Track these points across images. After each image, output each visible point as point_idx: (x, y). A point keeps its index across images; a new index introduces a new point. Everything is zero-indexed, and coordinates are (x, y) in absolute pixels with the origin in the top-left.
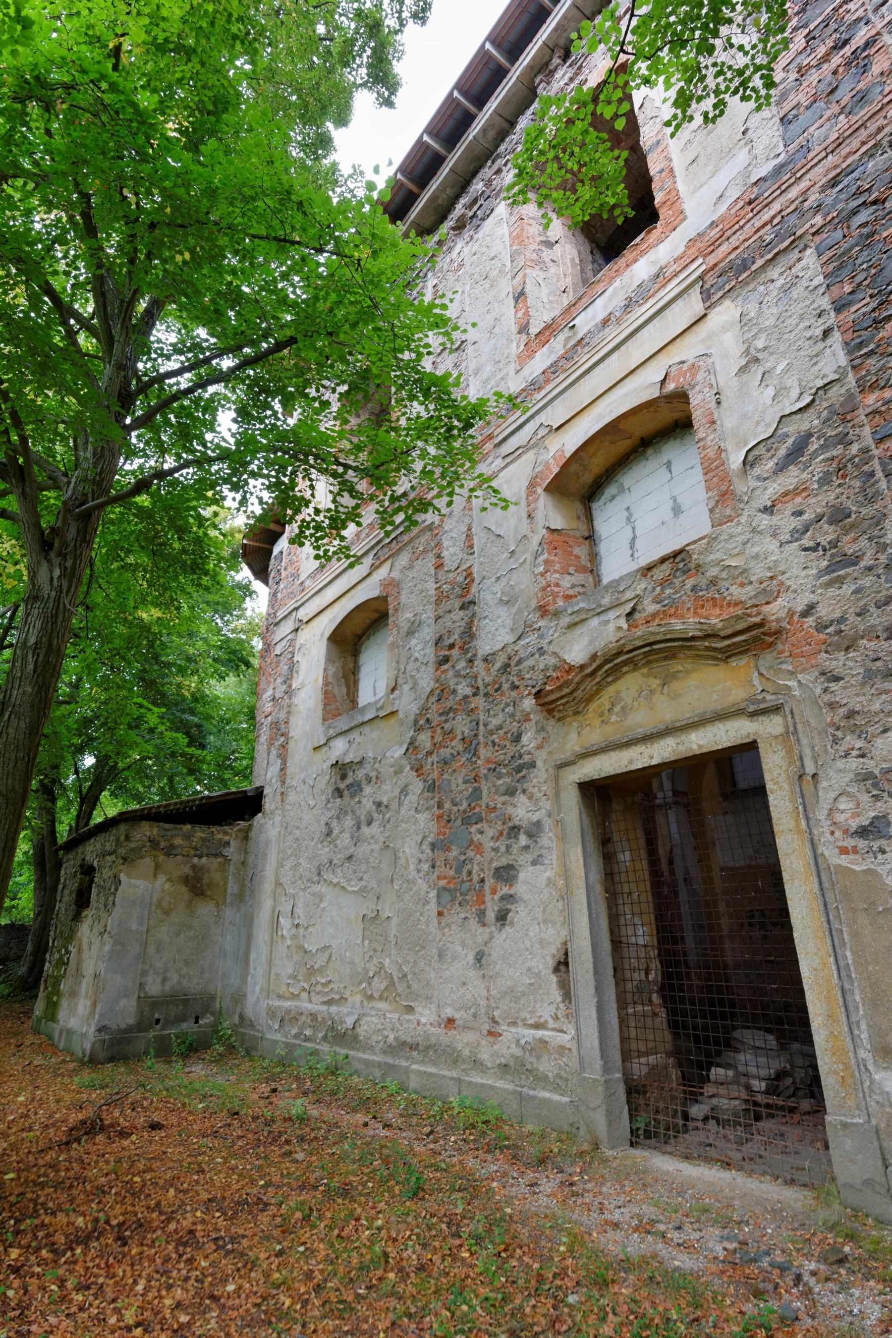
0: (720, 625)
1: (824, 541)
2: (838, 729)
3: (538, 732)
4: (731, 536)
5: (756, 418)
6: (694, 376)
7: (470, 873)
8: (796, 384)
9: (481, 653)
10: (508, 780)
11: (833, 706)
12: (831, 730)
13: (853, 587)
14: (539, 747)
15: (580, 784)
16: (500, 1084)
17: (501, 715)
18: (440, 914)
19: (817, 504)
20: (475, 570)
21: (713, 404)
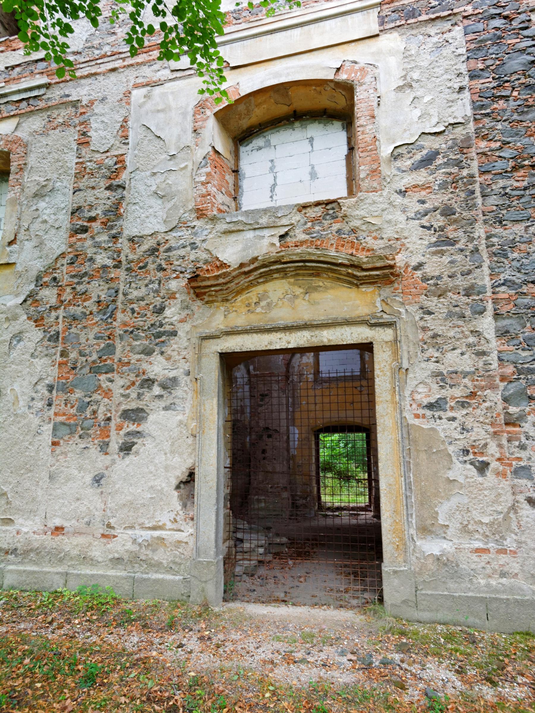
0: (365, 260)
1: (436, 225)
2: (425, 343)
3: (183, 309)
4: (374, 203)
5: (405, 127)
6: (363, 77)
7: (94, 412)
8: (436, 114)
9: (126, 233)
10: (147, 343)
11: (424, 329)
12: (421, 344)
13: (449, 259)
14: (181, 321)
15: (221, 354)
16: (111, 573)
17: (143, 289)
18: (54, 444)
19: (437, 199)
20: (128, 160)
21: (375, 104)
